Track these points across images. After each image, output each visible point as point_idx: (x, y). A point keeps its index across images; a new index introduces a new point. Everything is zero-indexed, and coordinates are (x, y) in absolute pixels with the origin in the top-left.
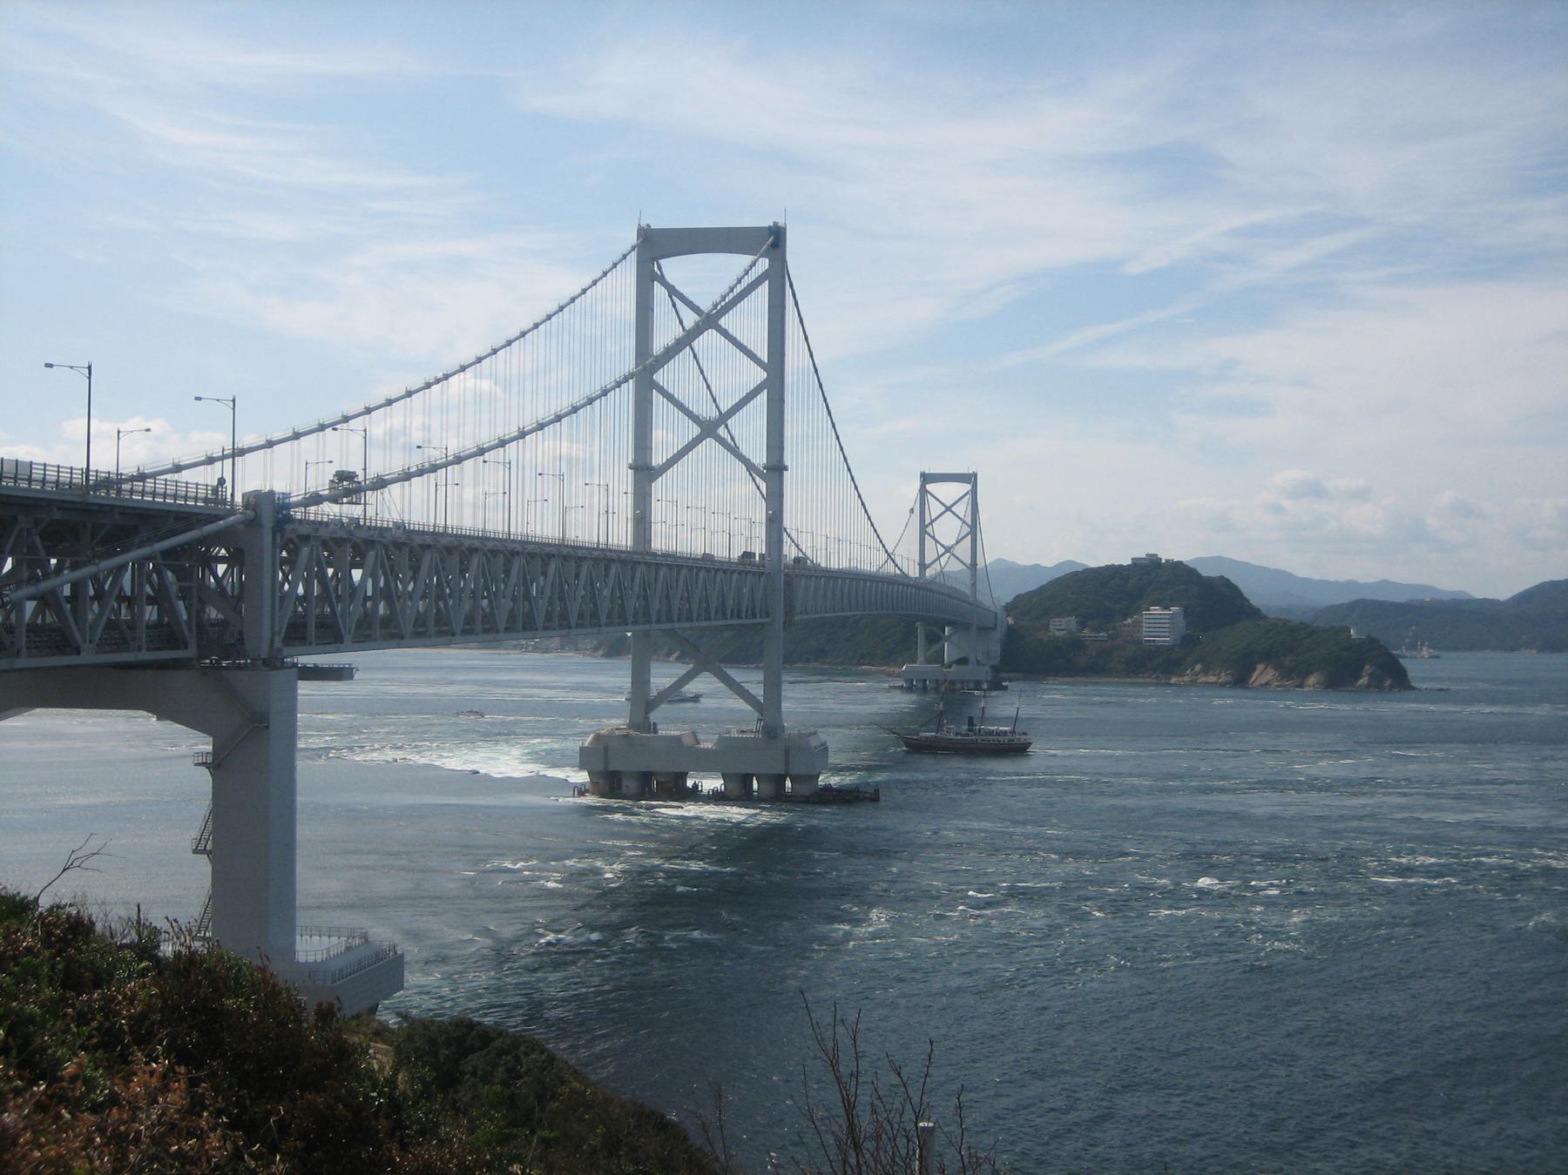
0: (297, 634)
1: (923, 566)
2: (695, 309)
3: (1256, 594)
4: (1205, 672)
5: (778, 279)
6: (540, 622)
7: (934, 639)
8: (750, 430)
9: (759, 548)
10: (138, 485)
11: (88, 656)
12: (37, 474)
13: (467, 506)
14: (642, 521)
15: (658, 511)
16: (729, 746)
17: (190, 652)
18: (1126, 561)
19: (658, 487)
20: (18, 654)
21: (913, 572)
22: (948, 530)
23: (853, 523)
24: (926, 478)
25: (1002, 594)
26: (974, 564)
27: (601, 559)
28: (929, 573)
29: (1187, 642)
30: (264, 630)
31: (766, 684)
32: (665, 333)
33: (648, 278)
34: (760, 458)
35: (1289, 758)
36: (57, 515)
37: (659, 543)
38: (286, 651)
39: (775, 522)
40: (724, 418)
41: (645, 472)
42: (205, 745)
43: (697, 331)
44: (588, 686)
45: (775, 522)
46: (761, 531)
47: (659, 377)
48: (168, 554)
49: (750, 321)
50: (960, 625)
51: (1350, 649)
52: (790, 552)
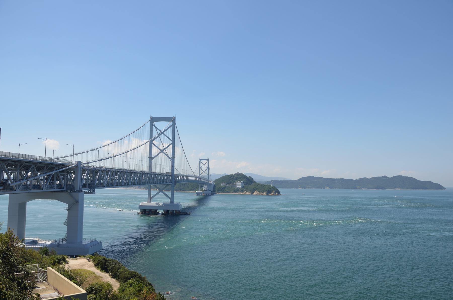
0: (84, 186)
1: (200, 174)
2: (160, 131)
3: (256, 179)
4: (247, 192)
5: (174, 125)
6: (136, 183)
7: (202, 187)
8: (169, 151)
9: (170, 171)
10: (57, 160)
11: (45, 190)
12: (35, 158)
13: (118, 165)
14: (150, 167)
15: (153, 165)
16: (165, 205)
17: (65, 189)
18: (234, 174)
19: (153, 161)
20: (31, 190)
21: (198, 175)
22: (204, 168)
23: (187, 167)
24: (201, 160)
25: (212, 180)
26: (208, 174)
27: (142, 173)
28: (201, 176)
29: (243, 187)
30: (78, 186)
31: (171, 195)
32: (155, 134)
33: (152, 125)
34: (171, 156)
35: (259, 203)
36: (51, 166)
37: (153, 170)
38: (82, 189)
39: (173, 167)
40: (165, 149)
41: (151, 158)
42: (66, 205)
43: (160, 135)
44: (140, 196)
45: (173, 167)
46: (170, 168)
47: (154, 142)
48: (60, 172)
49: (169, 133)
50: (206, 184)
51: (270, 189)
52: (175, 173)
